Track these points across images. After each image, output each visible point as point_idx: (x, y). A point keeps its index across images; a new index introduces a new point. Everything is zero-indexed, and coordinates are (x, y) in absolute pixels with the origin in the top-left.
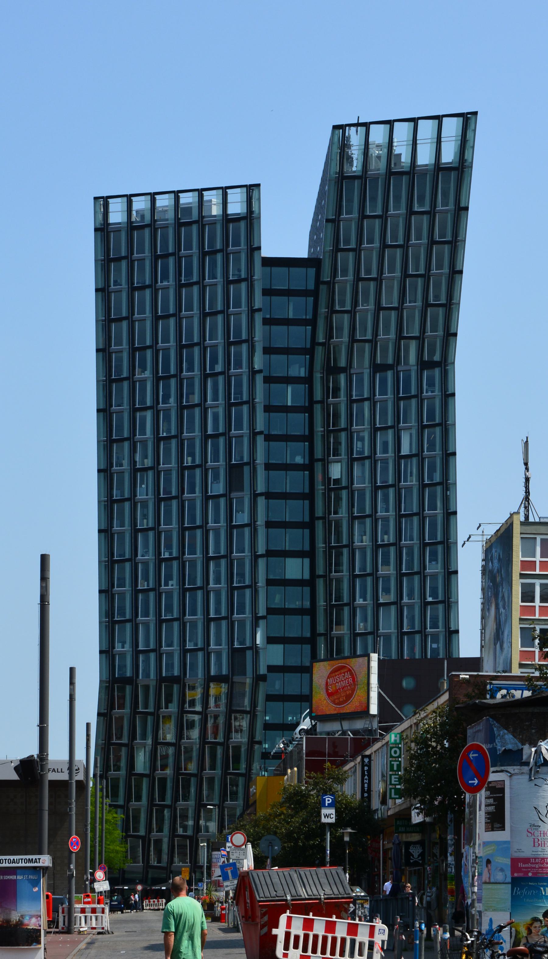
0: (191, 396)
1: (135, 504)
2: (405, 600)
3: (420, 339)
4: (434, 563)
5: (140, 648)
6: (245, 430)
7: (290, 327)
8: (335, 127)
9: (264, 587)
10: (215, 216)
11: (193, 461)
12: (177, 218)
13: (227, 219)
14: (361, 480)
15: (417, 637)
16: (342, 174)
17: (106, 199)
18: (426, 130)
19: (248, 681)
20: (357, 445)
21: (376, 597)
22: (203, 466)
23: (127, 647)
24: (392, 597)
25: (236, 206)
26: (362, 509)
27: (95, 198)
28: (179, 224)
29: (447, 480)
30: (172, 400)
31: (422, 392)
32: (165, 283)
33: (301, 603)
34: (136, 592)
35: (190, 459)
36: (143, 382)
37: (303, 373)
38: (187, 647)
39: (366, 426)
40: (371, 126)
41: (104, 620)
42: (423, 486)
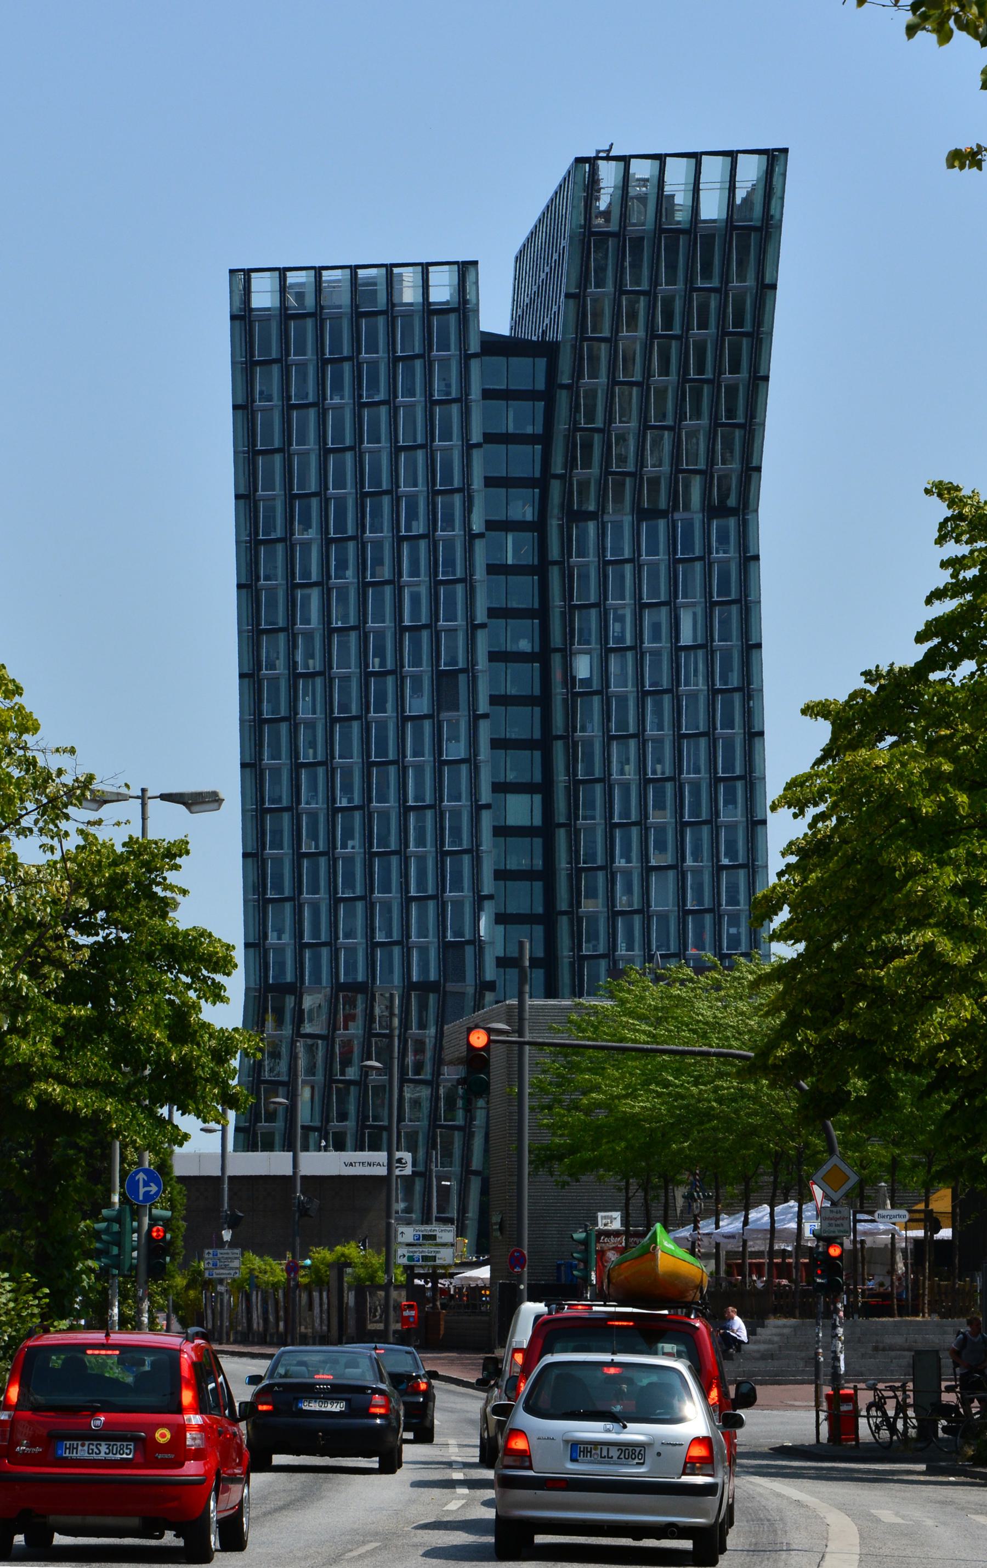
0: (378, 568)
1: (296, 726)
2: (689, 862)
3: (707, 474)
4: (730, 807)
5: (306, 940)
6: (460, 622)
7: (510, 446)
8: (579, 161)
9: (491, 852)
10: (411, 304)
11: (383, 663)
12: (354, 305)
13: (429, 310)
14: (622, 685)
15: (708, 918)
16: (590, 228)
17: (248, 272)
18: (713, 170)
19: (470, 990)
20: (614, 628)
21: (644, 857)
22: (397, 672)
23: (287, 939)
24: (669, 858)
25: (441, 293)
26: (623, 724)
27: (232, 271)
28: (357, 315)
29: (749, 683)
30: (350, 573)
31: (710, 553)
32: (337, 400)
33: (529, 862)
34: (299, 856)
35: (377, 660)
36: (306, 545)
37: (528, 514)
38: (377, 940)
39: (628, 601)
40: (632, 160)
41: (251, 897)
42: (714, 692)
